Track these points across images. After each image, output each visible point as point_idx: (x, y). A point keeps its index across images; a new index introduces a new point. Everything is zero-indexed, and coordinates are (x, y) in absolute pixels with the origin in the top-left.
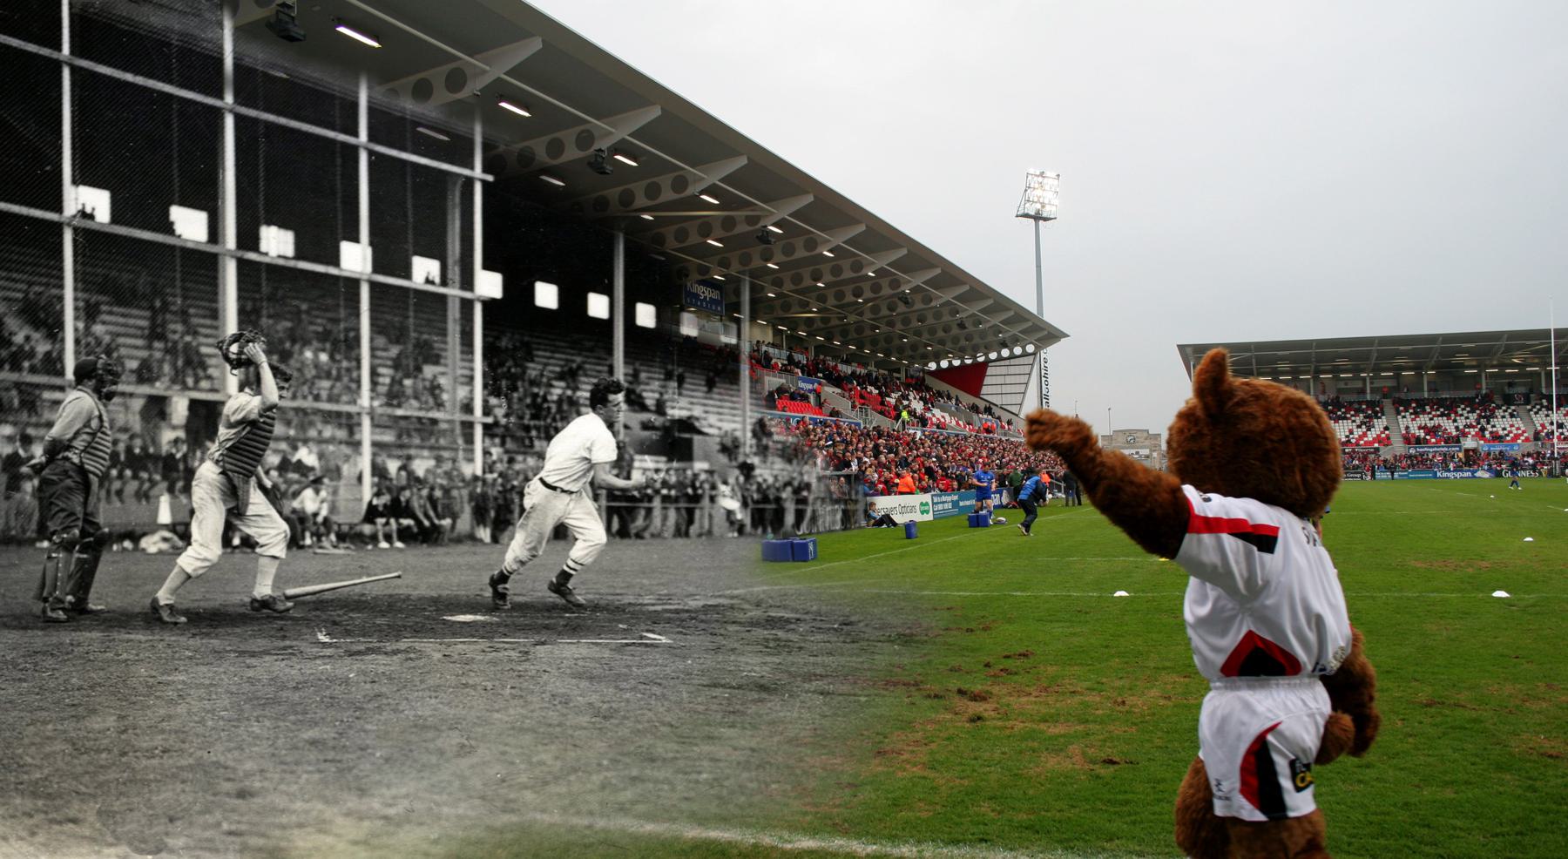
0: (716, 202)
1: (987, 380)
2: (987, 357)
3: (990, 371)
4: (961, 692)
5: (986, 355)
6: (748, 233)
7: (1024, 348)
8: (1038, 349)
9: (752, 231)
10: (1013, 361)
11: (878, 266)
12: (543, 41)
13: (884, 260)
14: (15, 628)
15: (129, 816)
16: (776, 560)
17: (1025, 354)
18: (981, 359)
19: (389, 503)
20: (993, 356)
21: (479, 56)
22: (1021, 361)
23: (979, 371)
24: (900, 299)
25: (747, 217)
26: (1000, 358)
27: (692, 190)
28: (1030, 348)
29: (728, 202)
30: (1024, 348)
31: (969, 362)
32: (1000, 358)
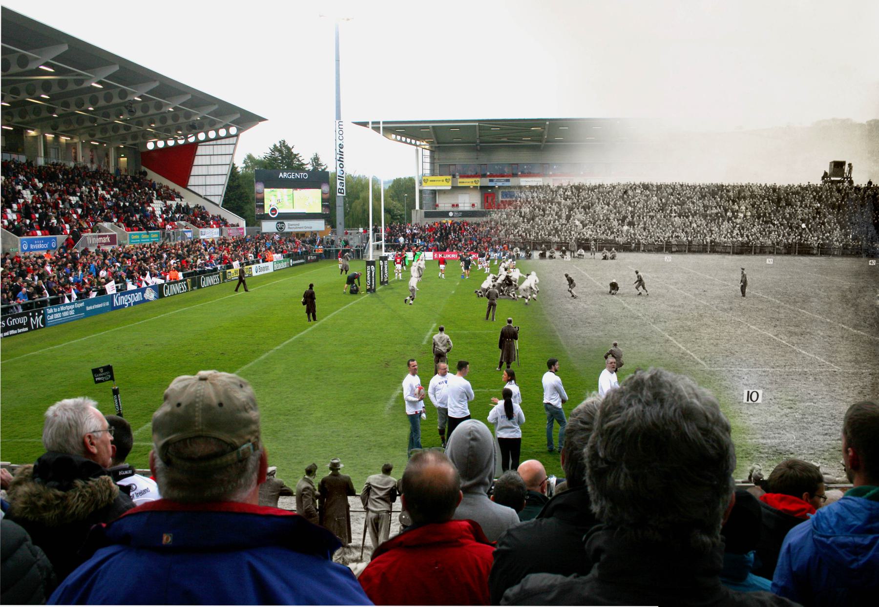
0: (52, 70)
1: (198, 160)
2: (197, 138)
3: (201, 150)
4: (426, 431)
5: (196, 135)
6: (75, 90)
7: (217, 132)
8: (240, 131)
9: (123, 103)
10: (219, 142)
11: (202, 114)
12: (69, 45)
13: (178, 102)
14: (223, 441)
15: (407, 336)
16: (554, 124)
17: (228, 136)
18: (192, 140)
19: (96, 403)
20: (202, 136)
21: (167, 99)
22: (227, 141)
23: (190, 151)
24: (126, 107)
25: (75, 80)
26: (208, 140)
27: (32, 66)
28: (233, 130)
29: (59, 71)
30: (217, 132)
31: (181, 142)
32: (208, 140)
